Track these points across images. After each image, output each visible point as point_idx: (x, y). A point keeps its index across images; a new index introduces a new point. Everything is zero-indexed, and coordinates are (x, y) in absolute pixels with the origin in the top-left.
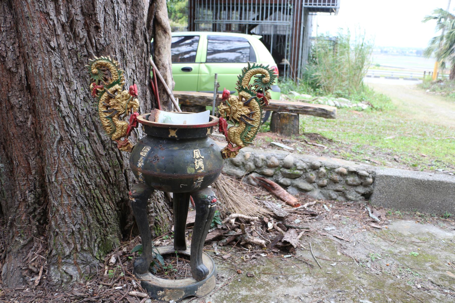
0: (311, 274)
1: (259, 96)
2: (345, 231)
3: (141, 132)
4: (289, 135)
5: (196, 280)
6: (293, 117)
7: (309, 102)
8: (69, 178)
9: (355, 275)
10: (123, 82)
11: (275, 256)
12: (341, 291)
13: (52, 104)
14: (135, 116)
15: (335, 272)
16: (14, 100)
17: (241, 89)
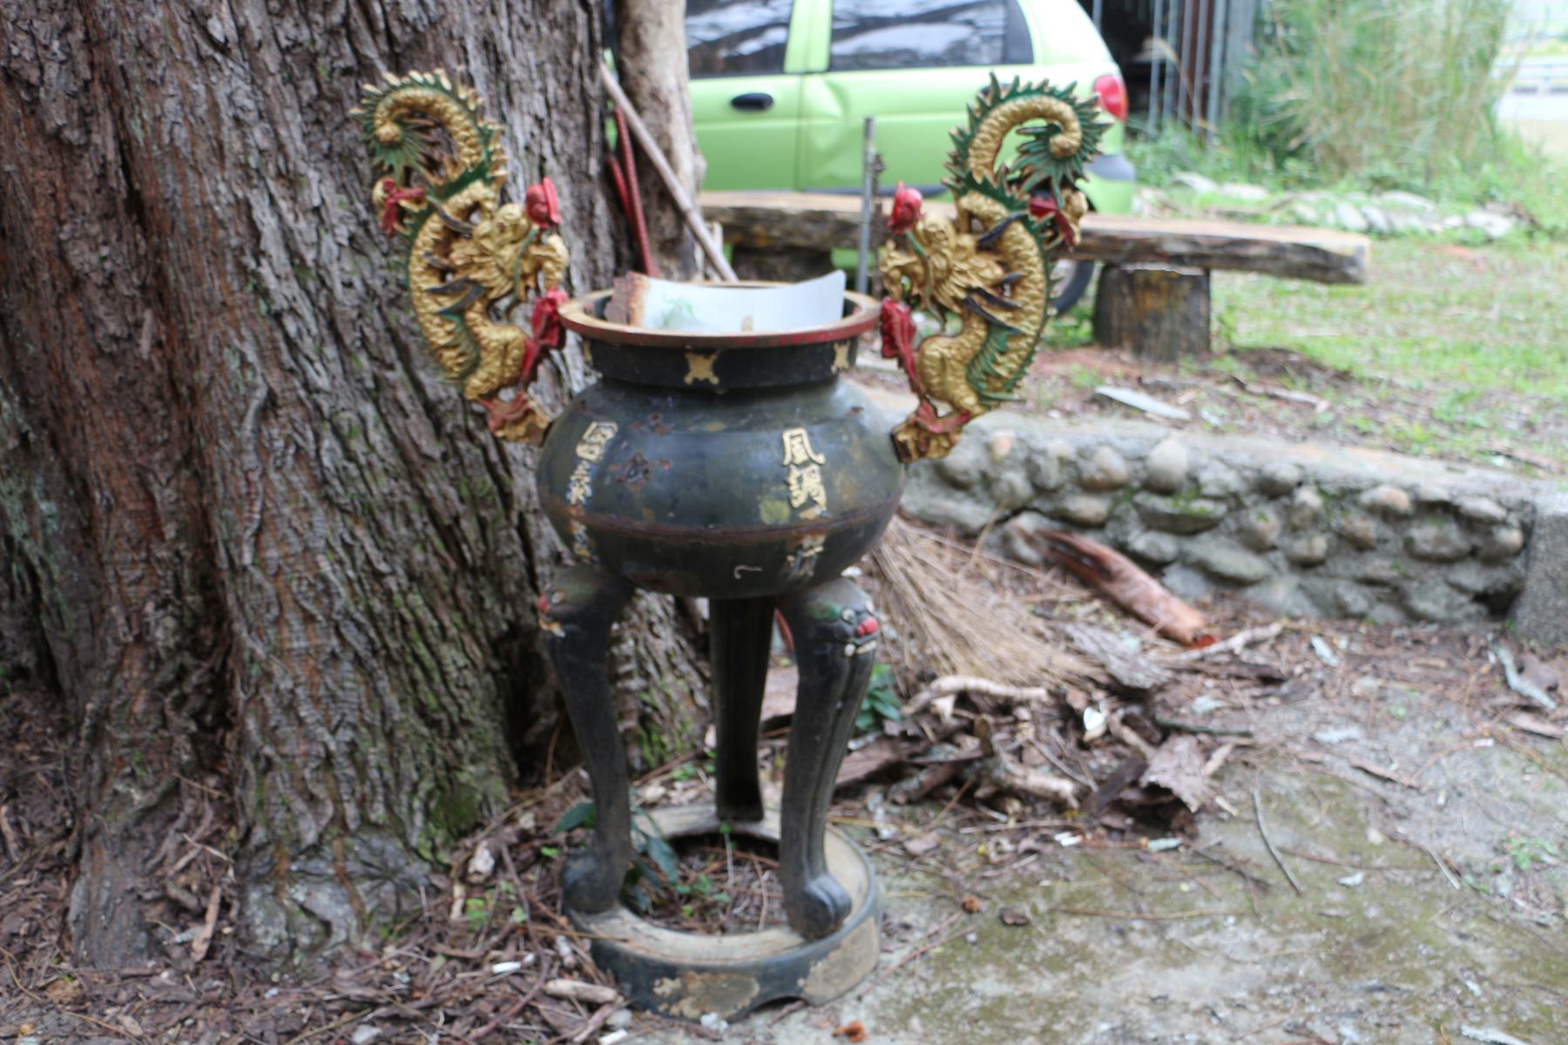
0: (1257, 916)
1: (1039, 211)
2: (1402, 748)
3: (578, 372)
4: (1168, 357)
5: (804, 936)
6: (1186, 286)
7: (1255, 218)
8: (306, 549)
9: (1443, 926)
10: (501, 172)
11: (1112, 844)
12: (1381, 989)
13: (230, 267)
14: (553, 302)
15: (1359, 911)
16: (82, 257)
17: (966, 184)
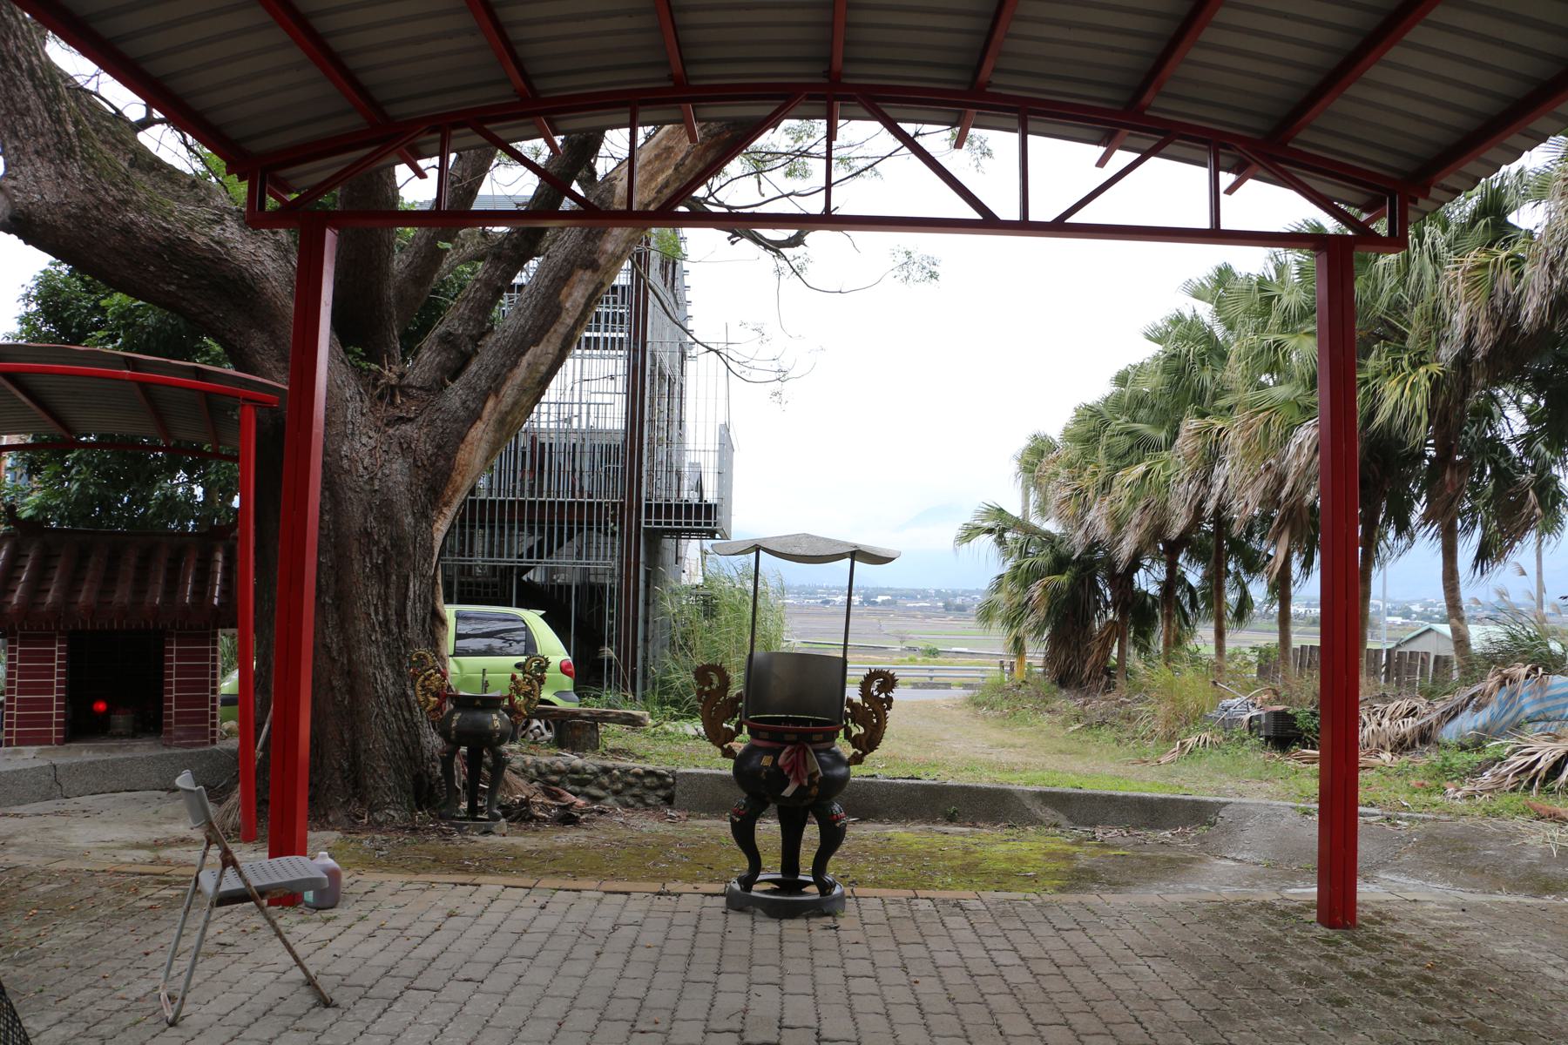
16: (335, 683)
